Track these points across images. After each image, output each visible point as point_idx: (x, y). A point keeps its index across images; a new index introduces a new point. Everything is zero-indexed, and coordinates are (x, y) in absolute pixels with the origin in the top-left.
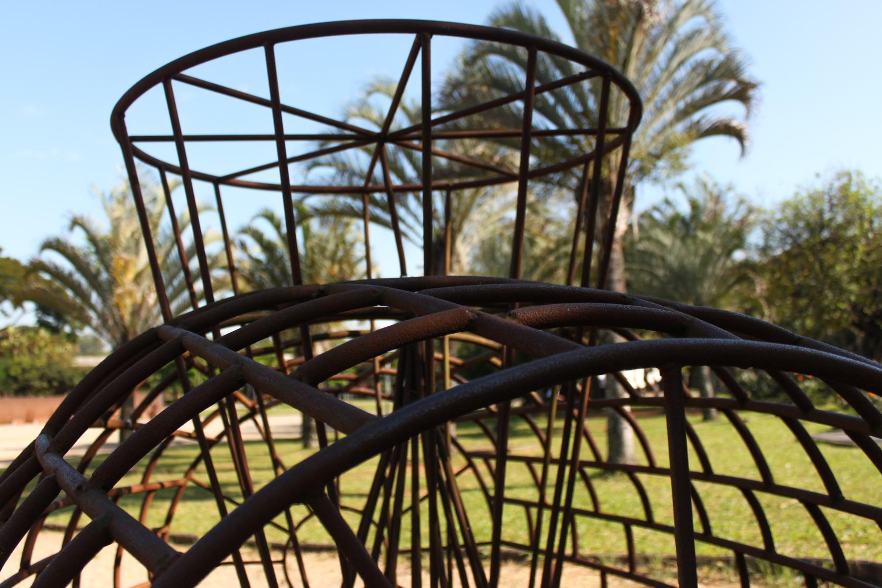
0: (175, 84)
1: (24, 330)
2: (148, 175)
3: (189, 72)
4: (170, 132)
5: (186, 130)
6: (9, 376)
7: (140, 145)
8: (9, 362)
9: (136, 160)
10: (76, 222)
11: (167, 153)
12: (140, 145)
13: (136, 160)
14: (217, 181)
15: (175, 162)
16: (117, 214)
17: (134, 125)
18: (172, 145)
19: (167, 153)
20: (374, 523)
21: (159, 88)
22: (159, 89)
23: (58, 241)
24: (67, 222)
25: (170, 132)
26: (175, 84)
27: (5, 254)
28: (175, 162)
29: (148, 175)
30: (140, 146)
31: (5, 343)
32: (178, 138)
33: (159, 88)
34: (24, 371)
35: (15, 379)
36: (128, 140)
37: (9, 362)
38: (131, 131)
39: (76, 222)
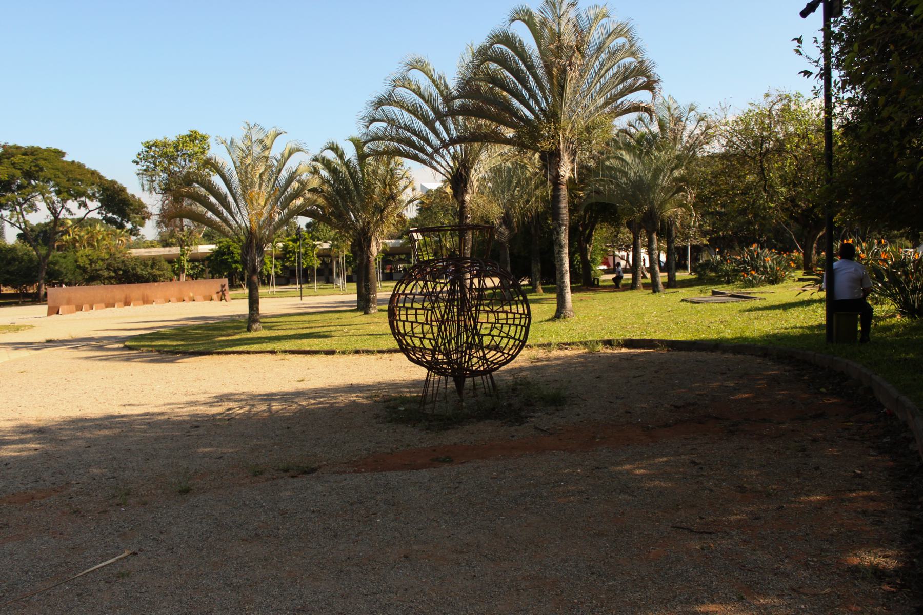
35: (84, 269)
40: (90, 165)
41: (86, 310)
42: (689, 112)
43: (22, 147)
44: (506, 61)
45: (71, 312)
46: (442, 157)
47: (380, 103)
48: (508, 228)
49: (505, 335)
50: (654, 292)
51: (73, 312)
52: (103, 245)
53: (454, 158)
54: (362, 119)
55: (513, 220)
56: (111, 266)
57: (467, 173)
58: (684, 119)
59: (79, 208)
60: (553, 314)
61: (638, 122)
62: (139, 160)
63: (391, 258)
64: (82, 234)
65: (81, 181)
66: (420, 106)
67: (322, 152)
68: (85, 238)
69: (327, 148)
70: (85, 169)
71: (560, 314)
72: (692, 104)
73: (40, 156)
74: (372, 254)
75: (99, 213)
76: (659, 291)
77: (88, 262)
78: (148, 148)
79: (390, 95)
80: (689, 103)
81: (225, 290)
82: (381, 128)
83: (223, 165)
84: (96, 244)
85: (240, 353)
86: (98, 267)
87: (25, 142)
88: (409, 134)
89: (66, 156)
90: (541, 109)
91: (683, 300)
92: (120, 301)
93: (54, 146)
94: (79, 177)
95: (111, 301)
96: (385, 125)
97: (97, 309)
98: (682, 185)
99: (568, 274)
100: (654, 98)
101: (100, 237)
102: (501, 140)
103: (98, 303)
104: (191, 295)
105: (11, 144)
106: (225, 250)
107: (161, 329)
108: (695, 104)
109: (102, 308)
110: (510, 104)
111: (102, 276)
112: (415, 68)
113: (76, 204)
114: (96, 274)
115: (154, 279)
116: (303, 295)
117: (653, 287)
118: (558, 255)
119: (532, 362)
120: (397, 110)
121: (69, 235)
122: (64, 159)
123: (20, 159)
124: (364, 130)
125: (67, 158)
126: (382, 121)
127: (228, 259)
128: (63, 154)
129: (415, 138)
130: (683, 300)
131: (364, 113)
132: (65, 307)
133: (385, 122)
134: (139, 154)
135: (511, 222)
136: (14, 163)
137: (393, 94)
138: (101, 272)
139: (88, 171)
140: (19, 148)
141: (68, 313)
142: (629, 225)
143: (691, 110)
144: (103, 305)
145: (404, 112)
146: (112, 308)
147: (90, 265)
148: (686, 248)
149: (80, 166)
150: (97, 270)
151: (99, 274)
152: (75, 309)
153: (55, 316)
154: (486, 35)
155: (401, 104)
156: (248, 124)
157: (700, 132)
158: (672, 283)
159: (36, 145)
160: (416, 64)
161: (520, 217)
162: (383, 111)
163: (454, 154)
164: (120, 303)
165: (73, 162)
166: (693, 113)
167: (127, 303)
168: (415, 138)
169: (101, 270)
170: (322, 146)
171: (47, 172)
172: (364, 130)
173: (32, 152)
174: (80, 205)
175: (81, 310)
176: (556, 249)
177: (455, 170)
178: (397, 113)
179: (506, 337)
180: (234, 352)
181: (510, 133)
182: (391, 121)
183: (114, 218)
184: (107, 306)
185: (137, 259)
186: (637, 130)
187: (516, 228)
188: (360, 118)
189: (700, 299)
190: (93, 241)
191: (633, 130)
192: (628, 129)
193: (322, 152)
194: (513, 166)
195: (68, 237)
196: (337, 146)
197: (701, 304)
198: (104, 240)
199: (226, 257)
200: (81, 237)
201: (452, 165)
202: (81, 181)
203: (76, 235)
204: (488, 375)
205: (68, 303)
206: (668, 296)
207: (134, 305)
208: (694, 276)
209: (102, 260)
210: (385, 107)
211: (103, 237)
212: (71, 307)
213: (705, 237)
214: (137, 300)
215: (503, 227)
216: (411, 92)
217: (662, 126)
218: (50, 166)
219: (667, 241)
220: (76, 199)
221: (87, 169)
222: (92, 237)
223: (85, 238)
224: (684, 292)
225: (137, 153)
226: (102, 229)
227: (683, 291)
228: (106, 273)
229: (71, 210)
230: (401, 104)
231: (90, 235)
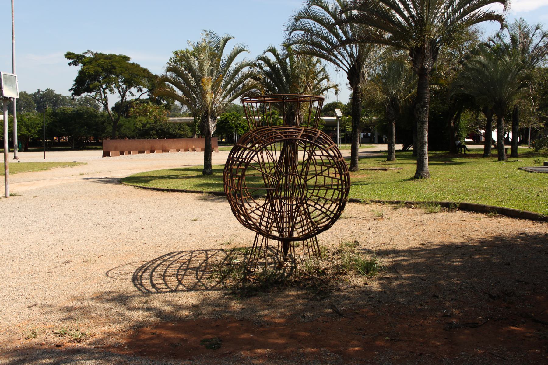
18: (332, 211)
40: (143, 66)
41: (126, 155)
42: (536, 30)
43: (105, 55)
45: (117, 155)
46: (340, 53)
47: (298, 18)
50: (500, 160)
51: (118, 155)
53: (351, 56)
54: (287, 29)
57: (360, 68)
58: (531, 35)
59: (138, 92)
60: (414, 174)
61: (496, 38)
62: (171, 63)
63: (331, 129)
66: (328, 19)
67: (264, 53)
69: (268, 51)
71: (419, 174)
72: (538, 24)
73: (114, 59)
75: (148, 95)
76: (503, 160)
77: (141, 125)
79: (307, 11)
80: (536, 24)
82: (300, 35)
87: (107, 52)
88: (320, 39)
89: (130, 60)
90: (411, 16)
91: (519, 169)
92: (148, 149)
93: (124, 54)
95: (142, 150)
96: (303, 32)
97: (133, 154)
98: (526, 82)
99: (427, 145)
100: (505, 9)
102: (380, 41)
103: (134, 150)
104: (194, 147)
105: (99, 53)
108: (541, 24)
109: (136, 154)
113: (136, 89)
115: (180, 137)
116: (276, 150)
117: (500, 157)
118: (419, 130)
120: (311, 22)
122: (129, 62)
123: (102, 61)
124: (288, 37)
125: (131, 61)
126: (301, 29)
128: (127, 59)
129: (323, 43)
130: (519, 169)
131: (288, 23)
132: (114, 152)
133: (303, 31)
134: (171, 59)
136: (99, 64)
139: (142, 69)
140: (103, 55)
141: (115, 156)
142: (485, 112)
143: (537, 28)
144: (137, 152)
145: (316, 23)
146: (143, 154)
148: (528, 129)
149: (137, 66)
152: (119, 153)
153: (107, 157)
155: (316, 19)
156: (205, 31)
157: (543, 45)
158: (515, 154)
159: (113, 53)
162: (301, 23)
165: (133, 63)
166: (538, 31)
167: (152, 151)
168: (323, 43)
170: (266, 48)
171: (118, 70)
172: (288, 37)
173: (111, 57)
175: (123, 154)
176: (419, 125)
178: (311, 24)
181: (388, 35)
182: (308, 31)
184: (140, 152)
185: (174, 124)
186: (495, 43)
188: (285, 27)
189: (534, 169)
191: (492, 44)
192: (488, 43)
193: (264, 53)
196: (275, 49)
197: (533, 173)
201: (349, 62)
204: (314, 238)
205: (115, 150)
206: (509, 164)
207: (156, 152)
208: (532, 149)
210: (302, 20)
212: (117, 152)
213: (542, 122)
214: (159, 149)
217: (513, 38)
218: (119, 66)
219: (513, 123)
220: (136, 87)
224: (522, 162)
225: (170, 59)
227: (521, 160)
230: (316, 19)
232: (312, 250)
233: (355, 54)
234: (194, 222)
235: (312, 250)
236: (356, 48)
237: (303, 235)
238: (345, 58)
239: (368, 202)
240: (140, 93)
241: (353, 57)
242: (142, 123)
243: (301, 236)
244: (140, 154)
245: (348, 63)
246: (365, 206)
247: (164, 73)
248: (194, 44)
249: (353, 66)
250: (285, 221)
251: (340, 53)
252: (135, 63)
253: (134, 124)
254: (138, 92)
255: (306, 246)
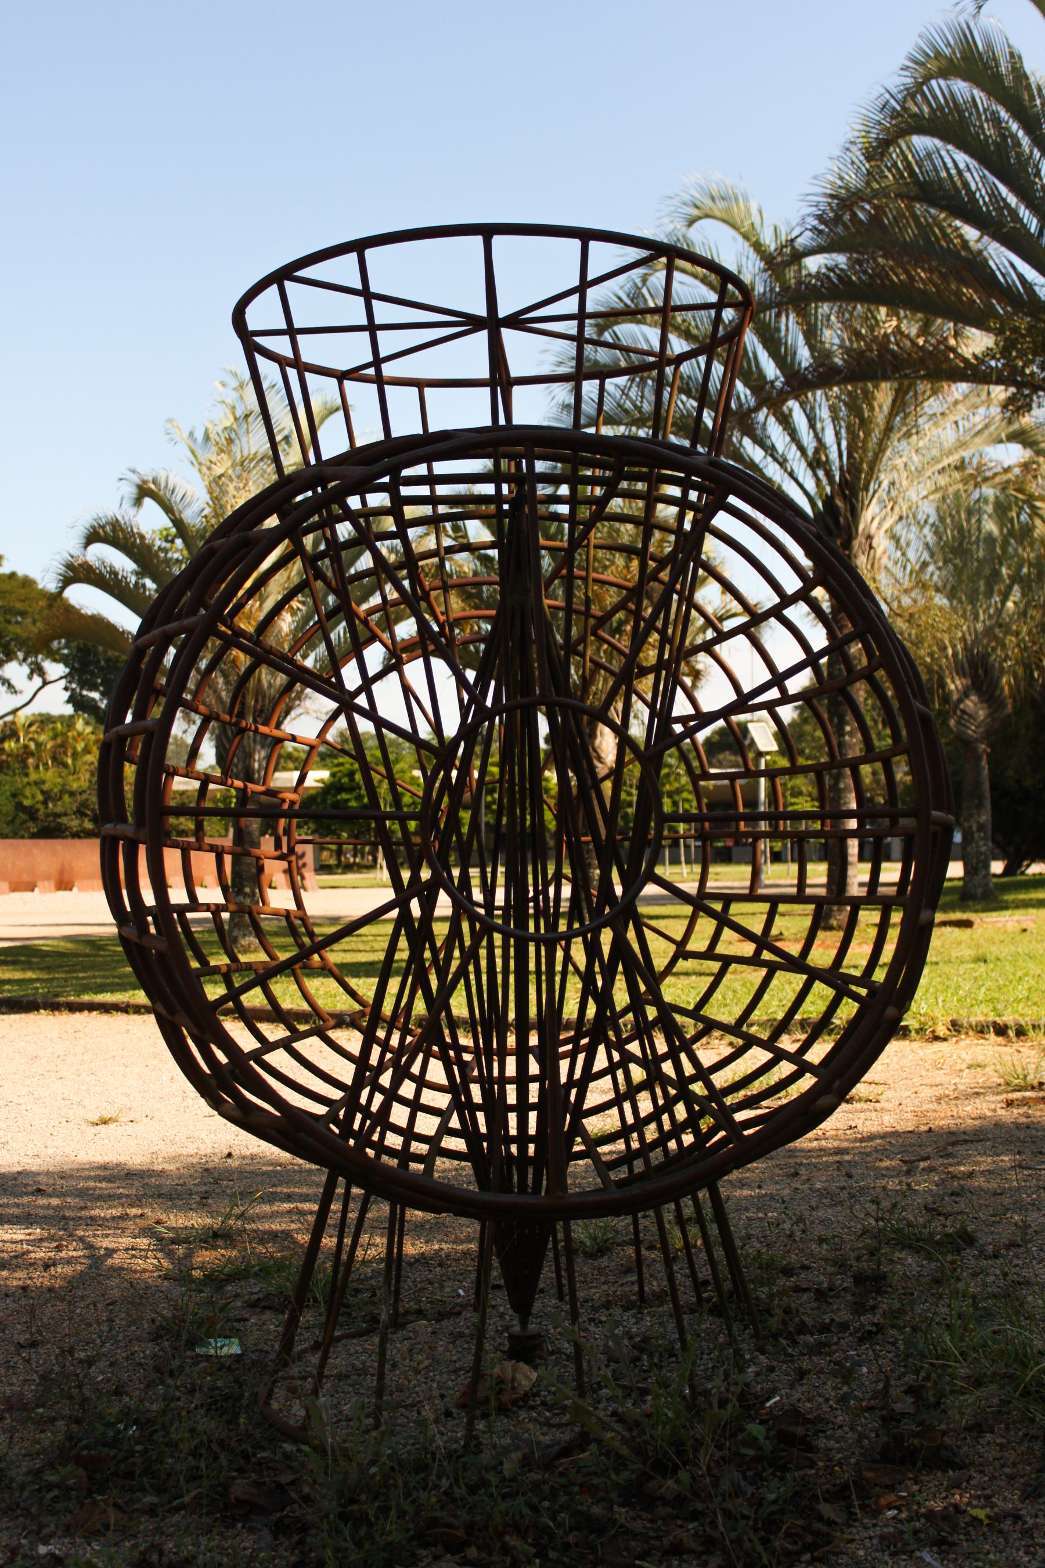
0: (288, 284)
1: (45, 721)
2: (268, 369)
3: (302, 273)
4: (283, 326)
5: (297, 324)
6: (20, 807)
7: (259, 340)
8: (20, 781)
9: (258, 357)
10: (144, 492)
11: (281, 345)
12: (259, 340)
13: (258, 357)
14: (342, 376)
15: (289, 354)
16: (218, 470)
17: (254, 320)
18: (286, 339)
19: (281, 345)
20: (567, 878)
21: (274, 288)
22: (273, 290)
23: (115, 524)
24: (130, 491)
25: (283, 326)
26: (288, 284)
27: (6, 569)
28: (289, 354)
29: (268, 369)
30: (260, 340)
31: (10, 745)
32: (292, 332)
33: (274, 288)
34: (48, 796)
35: (32, 813)
36: (402, 1171)
37: (20, 781)
38: (252, 326)
39: (144, 492)
44: (963, 123)
46: (786, 421)
48: (986, 702)
49: (748, 949)
52: (85, 763)
55: (999, 678)
56: (87, 807)
57: (855, 514)
59: (30, 677)
64: (43, 738)
65: (22, 614)
68: (49, 746)
70: (36, 589)
74: (600, 759)
75: (66, 689)
77: (40, 797)
78: (167, 541)
81: (304, 865)
83: (187, 499)
84: (70, 761)
85: (106, 1008)
86: (59, 809)
92: (47, 878)
94: (19, 606)
95: (26, 878)
101: (80, 747)
106: (345, 780)
107: (41, 942)
110: (985, 263)
111: (67, 828)
112: (707, 216)
113: (26, 670)
114: (53, 825)
119: (1010, 1104)
121: (18, 740)
127: (348, 800)
135: (995, 684)
137: (644, 291)
138: (64, 820)
146: (28, 895)
147: (45, 803)
150: (58, 815)
151: (60, 824)
154: (905, 53)
160: (709, 203)
161: (1020, 671)
163: (817, 451)
164: (46, 883)
165: (13, 575)
167: (64, 884)
169: (66, 814)
174: (32, 672)
177: (820, 504)
179: (754, 961)
180: (91, 1007)
183: (93, 700)
184: (15, 887)
187: (1009, 702)
190: (65, 753)
194: (1001, 530)
195: (13, 744)
198: (89, 752)
199: (345, 796)
200: (39, 745)
201: (810, 485)
202: (22, 614)
203: (31, 739)
204: (703, 1194)
209: (72, 794)
211: (86, 746)
215: (974, 698)
216: (697, 283)
221: (41, 590)
222: (64, 745)
223: (49, 746)
226: (89, 729)
228: (74, 823)
229: (13, 682)
231: (59, 740)
232: (693, 1274)
233: (834, 455)
234: (101, 1128)
235: (693, 1274)
236: (837, 434)
237: (633, 1178)
238: (792, 475)
239: (941, 1031)
240: (37, 681)
241: (826, 466)
242: (43, 792)
243: (621, 1184)
244: (16, 895)
245: (806, 493)
246: (938, 1046)
247: (77, 551)
248: (191, 434)
249: (828, 501)
250: (533, 1116)
251: (786, 421)
252: (20, 573)
253: (14, 795)
254: (30, 677)
255: (706, 1283)
